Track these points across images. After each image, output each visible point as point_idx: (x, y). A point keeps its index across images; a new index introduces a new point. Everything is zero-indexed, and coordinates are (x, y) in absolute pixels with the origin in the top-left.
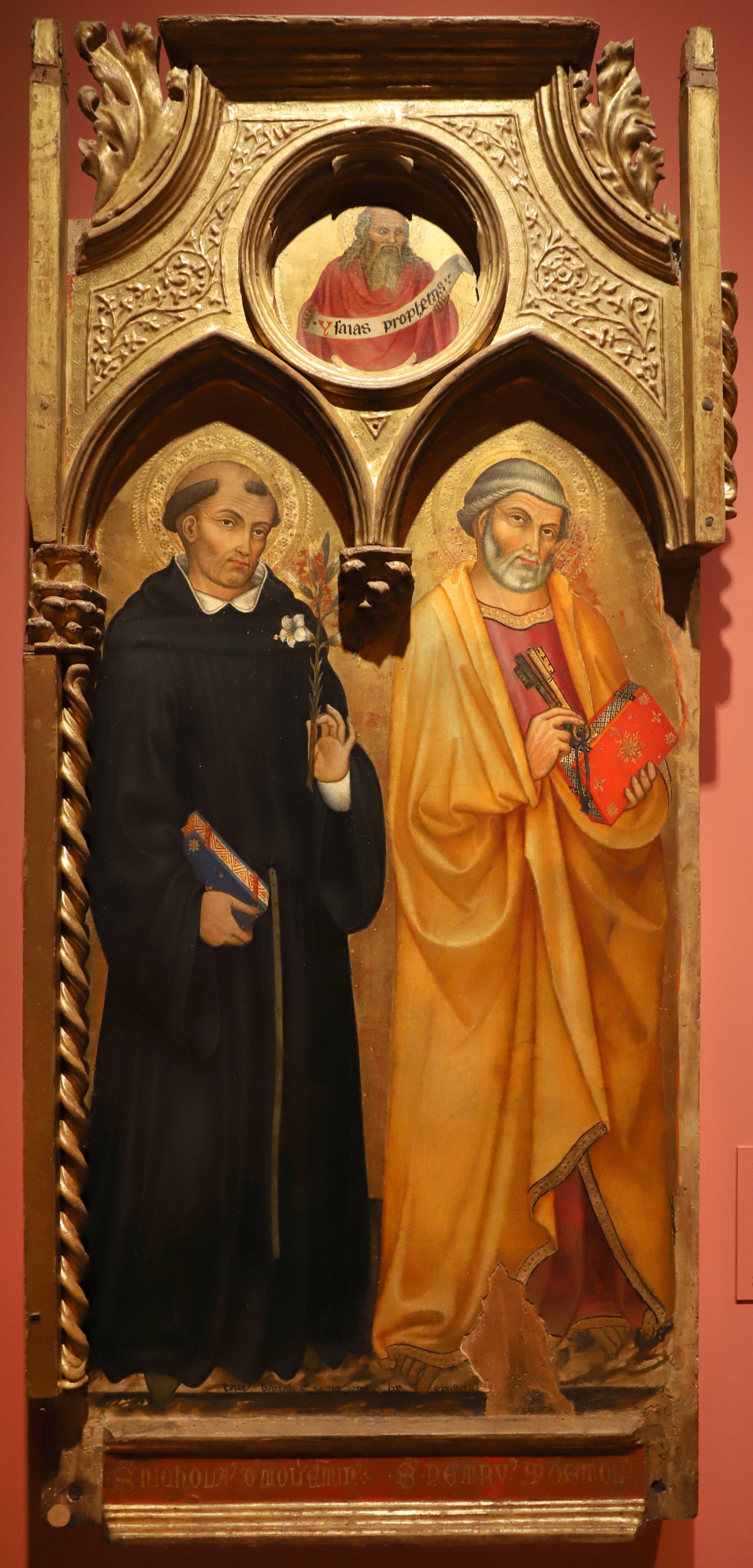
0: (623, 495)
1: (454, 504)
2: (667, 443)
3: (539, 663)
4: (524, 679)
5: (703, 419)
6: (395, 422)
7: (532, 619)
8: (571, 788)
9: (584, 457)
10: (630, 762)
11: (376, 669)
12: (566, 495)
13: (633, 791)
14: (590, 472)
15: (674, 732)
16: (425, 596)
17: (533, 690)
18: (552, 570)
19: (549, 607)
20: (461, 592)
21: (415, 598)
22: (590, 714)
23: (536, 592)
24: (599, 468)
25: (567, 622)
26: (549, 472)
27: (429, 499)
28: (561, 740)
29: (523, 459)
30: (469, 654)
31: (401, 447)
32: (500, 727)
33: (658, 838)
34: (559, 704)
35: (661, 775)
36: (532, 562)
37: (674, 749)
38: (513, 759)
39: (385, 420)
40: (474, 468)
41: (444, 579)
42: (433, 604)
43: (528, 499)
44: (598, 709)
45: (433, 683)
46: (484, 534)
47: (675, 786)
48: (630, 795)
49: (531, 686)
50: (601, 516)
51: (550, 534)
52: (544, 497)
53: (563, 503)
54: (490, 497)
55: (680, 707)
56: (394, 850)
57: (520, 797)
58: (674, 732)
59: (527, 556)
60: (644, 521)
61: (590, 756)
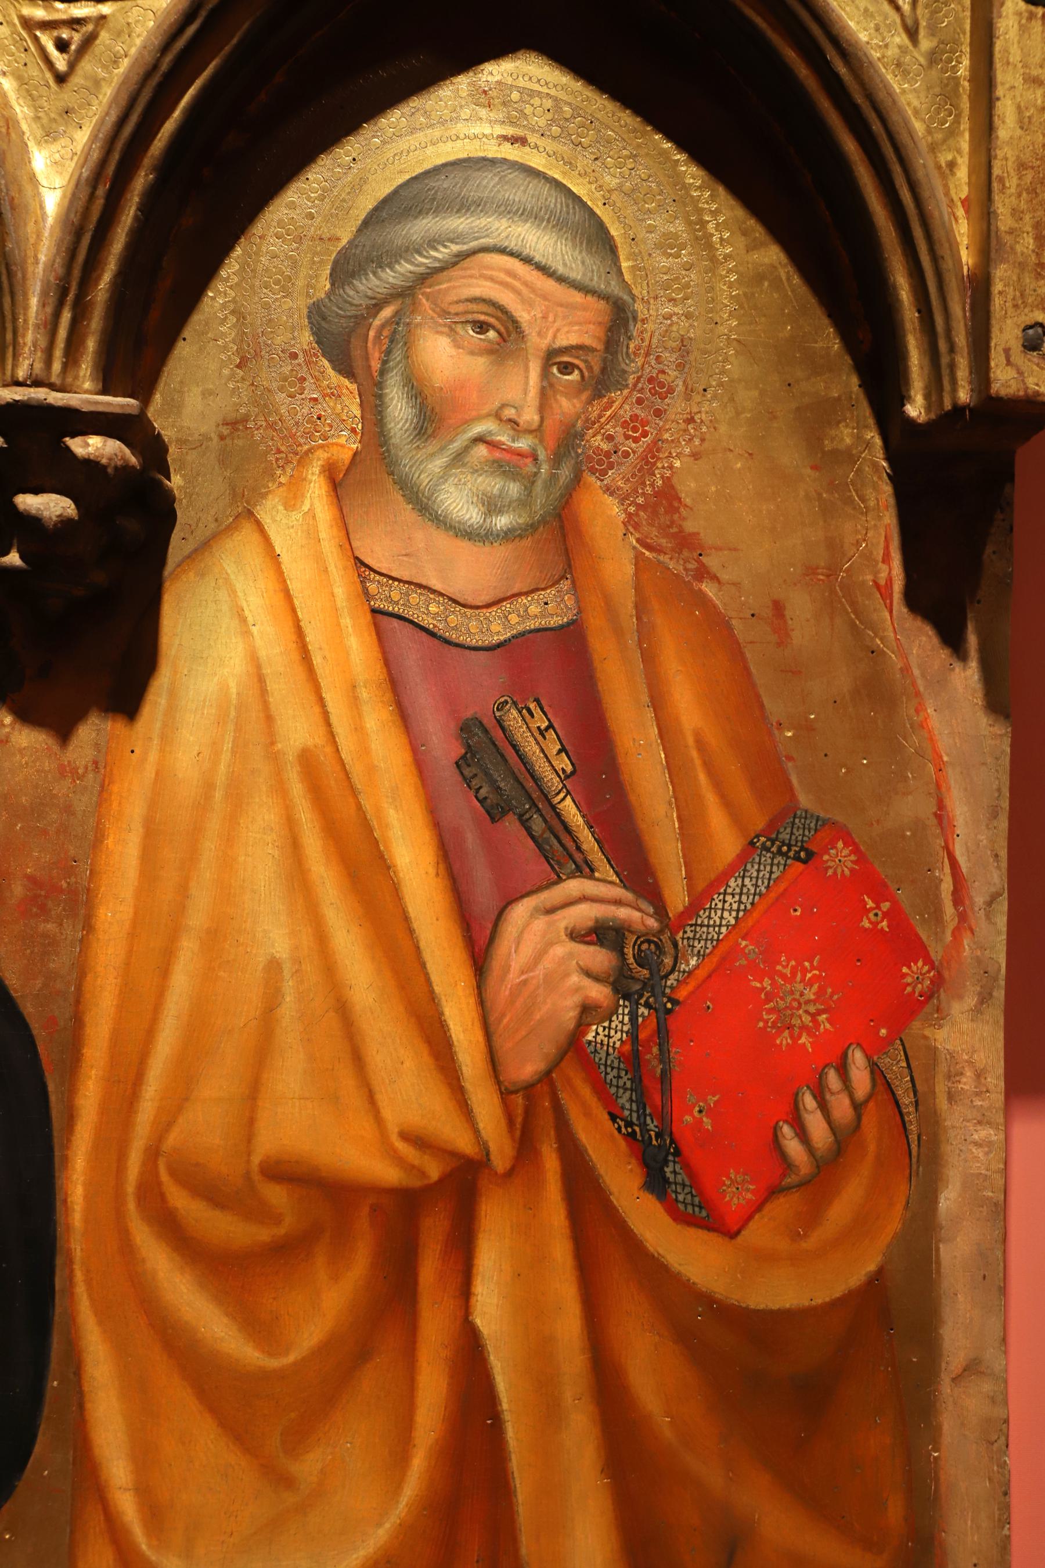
0: (790, 269)
1: (300, 283)
2: (916, 112)
3: (531, 748)
4: (483, 792)
5: (1023, 29)
6: (119, 34)
7: (514, 618)
8: (613, 1117)
9: (681, 157)
10: (795, 1047)
11: (56, 748)
12: (625, 265)
13: (802, 1134)
14: (695, 201)
15: (928, 961)
16: (206, 545)
17: (510, 824)
18: (577, 479)
19: (565, 585)
20: (312, 534)
21: (178, 547)
22: (677, 898)
23: (527, 542)
24: (721, 190)
25: (618, 632)
26: (577, 199)
27: (230, 269)
28: (588, 973)
29: (504, 161)
30: (326, 715)
31: (123, 101)
32: (411, 931)
33: (880, 1272)
34: (585, 869)
35: (889, 1086)
36: (520, 454)
37: (928, 1008)
38: (442, 1026)
39: (90, 27)
40: (364, 181)
41: (264, 496)
42: (229, 567)
43: (510, 273)
44: (701, 885)
45: (218, 795)
46: (382, 372)
47: (932, 1121)
48: (793, 1146)
49: (504, 813)
50: (722, 329)
51: (575, 376)
52: (561, 270)
53: (614, 288)
54: (405, 267)
55: (947, 886)
56: (81, 1289)
57: (464, 1143)
58: (928, 961)
59: (504, 438)
60: (850, 343)
61: (673, 1024)
